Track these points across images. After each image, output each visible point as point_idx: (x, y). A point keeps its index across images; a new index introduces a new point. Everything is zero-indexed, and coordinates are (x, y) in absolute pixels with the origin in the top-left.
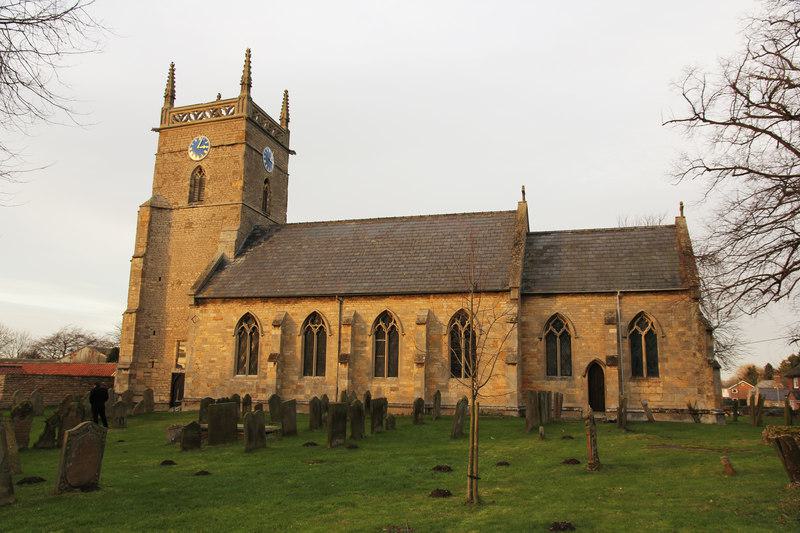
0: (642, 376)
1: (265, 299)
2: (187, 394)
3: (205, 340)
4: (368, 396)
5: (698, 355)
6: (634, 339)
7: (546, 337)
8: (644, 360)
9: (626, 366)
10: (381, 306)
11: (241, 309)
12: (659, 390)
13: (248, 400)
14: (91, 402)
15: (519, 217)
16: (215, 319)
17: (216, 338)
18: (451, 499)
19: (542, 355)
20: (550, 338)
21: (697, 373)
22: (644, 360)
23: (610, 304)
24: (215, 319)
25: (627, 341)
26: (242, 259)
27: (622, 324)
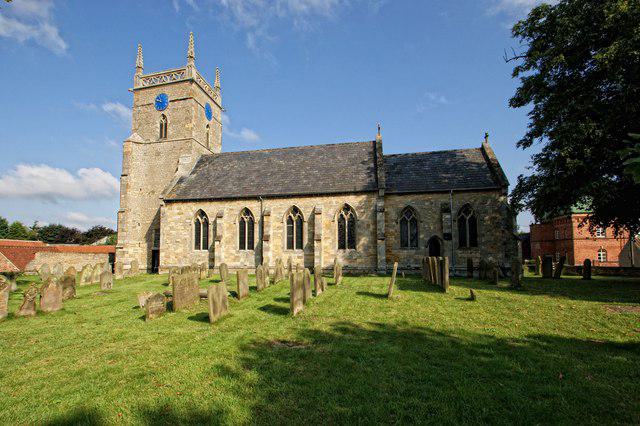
0: (465, 245)
1: (211, 200)
2: (162, 263)
3: (172, 228)
4: (360, 234)
5: (507, 232)
6: (462, 222)
7: (401, 221)
8: (468, 236)
9: (455, 240)
10: (292, 202)
11: (195, 207)
12: (478, 255)
13: (243, 22)
14: (33, 258)
15: (376, 147)
16: (179, 214)
17: (180, 226)
18: (262, 304)
19: (398, 234)
20: (403, 222)
21: (505, 244)
22: (468, 236)
23: (443, 199)
24: (179, 214)
25: (456, 223)
26: (194, 176)
27: (453, 212)
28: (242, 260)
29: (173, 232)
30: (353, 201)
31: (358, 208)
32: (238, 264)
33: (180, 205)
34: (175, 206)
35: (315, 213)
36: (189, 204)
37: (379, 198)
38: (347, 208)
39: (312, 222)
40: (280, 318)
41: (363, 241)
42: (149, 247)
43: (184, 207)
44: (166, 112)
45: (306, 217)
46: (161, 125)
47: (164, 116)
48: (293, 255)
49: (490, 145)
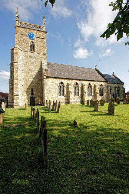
1: (65, 79)
11: (60, 81)
17: (53, 87)
28: (76, 100)
29: (50, 89)
30: (103, 84)
31: (104, 86)
32: (75, 101)
33: (53, 79)
34: (51, 79)
35: (68, 84)
36: (56, 79)
37: (108, 83)
38: (101, 85)
39: (68, 88)
40: (24, 111)
41: (105, 94)
42: (28, 96)
43: (54, 80)
44: (34, 41)
45: (93, 86)
46: (31, 46)
47: (32, 42)
48: (89, 98)
49: (115, 74)
